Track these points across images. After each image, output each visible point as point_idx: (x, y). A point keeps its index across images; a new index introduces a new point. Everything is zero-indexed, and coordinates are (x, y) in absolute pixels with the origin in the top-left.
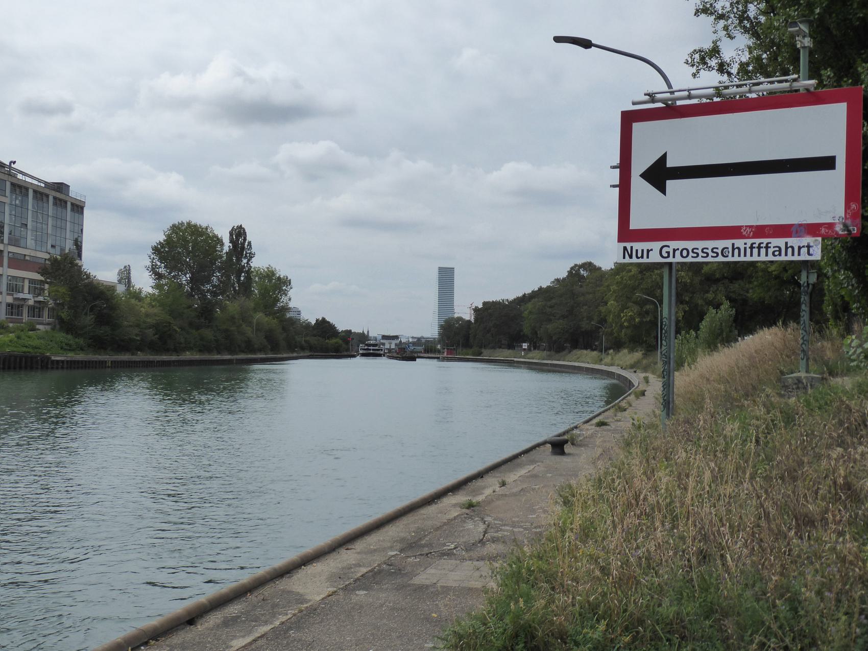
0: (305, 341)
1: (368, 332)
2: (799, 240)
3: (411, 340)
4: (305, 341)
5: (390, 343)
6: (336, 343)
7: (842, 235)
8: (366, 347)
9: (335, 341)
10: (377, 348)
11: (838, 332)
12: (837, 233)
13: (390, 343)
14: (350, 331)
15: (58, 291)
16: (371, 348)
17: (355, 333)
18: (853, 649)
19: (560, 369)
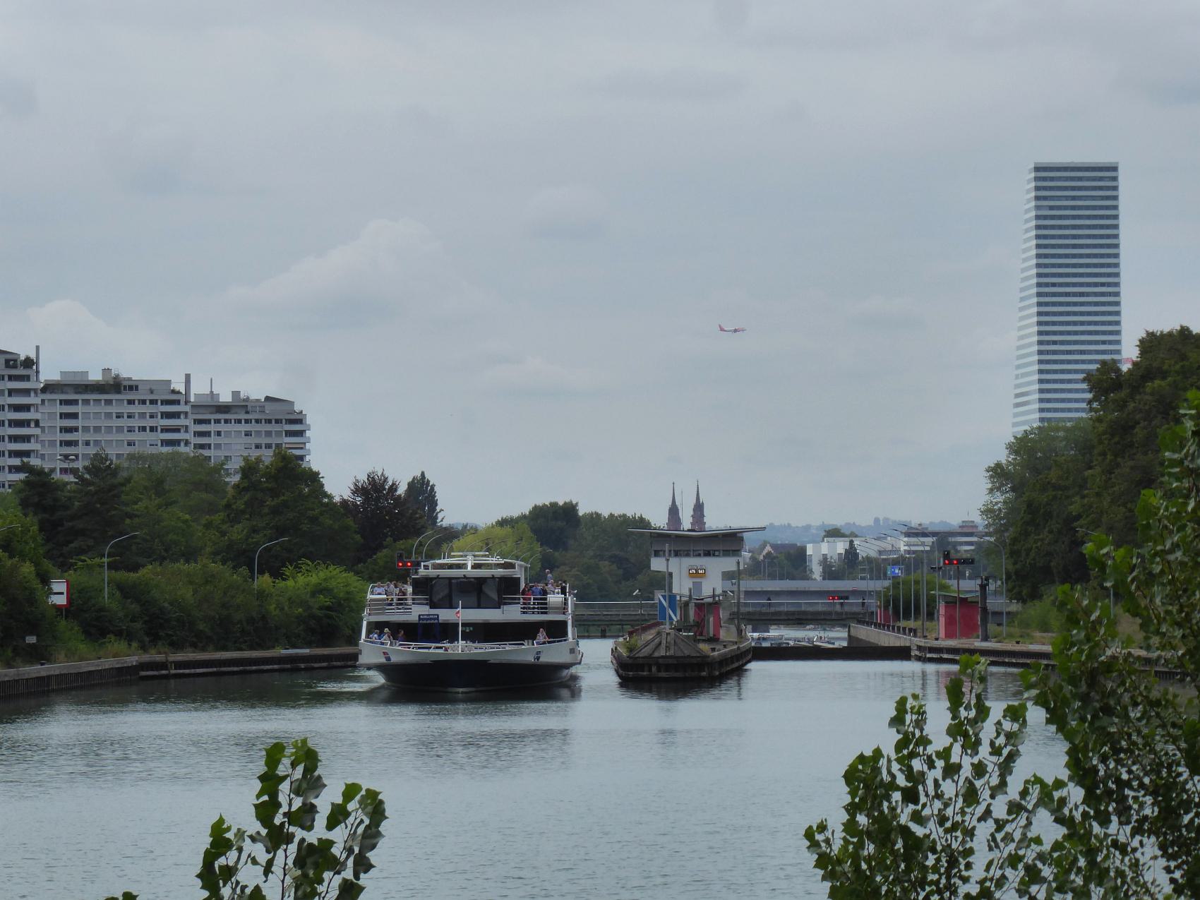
0: (125, 591)
1: (699, 508)
2: (278, 857)
3: (902, 545)
4: (125, 591)
5: (697, 574)
6: (319, 590)
7: (214, 867)
8: (417, 612)
9: (314, 579)
10: (512, 613)
11: (1085, 636)
12: (1082, 602)
13: (697, 574)
14: (567, 512)
15: (265, 535)
16: (461, 615)
17: (595, 518)
18: (997, 895)
19: (950, 656)
